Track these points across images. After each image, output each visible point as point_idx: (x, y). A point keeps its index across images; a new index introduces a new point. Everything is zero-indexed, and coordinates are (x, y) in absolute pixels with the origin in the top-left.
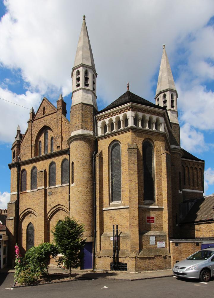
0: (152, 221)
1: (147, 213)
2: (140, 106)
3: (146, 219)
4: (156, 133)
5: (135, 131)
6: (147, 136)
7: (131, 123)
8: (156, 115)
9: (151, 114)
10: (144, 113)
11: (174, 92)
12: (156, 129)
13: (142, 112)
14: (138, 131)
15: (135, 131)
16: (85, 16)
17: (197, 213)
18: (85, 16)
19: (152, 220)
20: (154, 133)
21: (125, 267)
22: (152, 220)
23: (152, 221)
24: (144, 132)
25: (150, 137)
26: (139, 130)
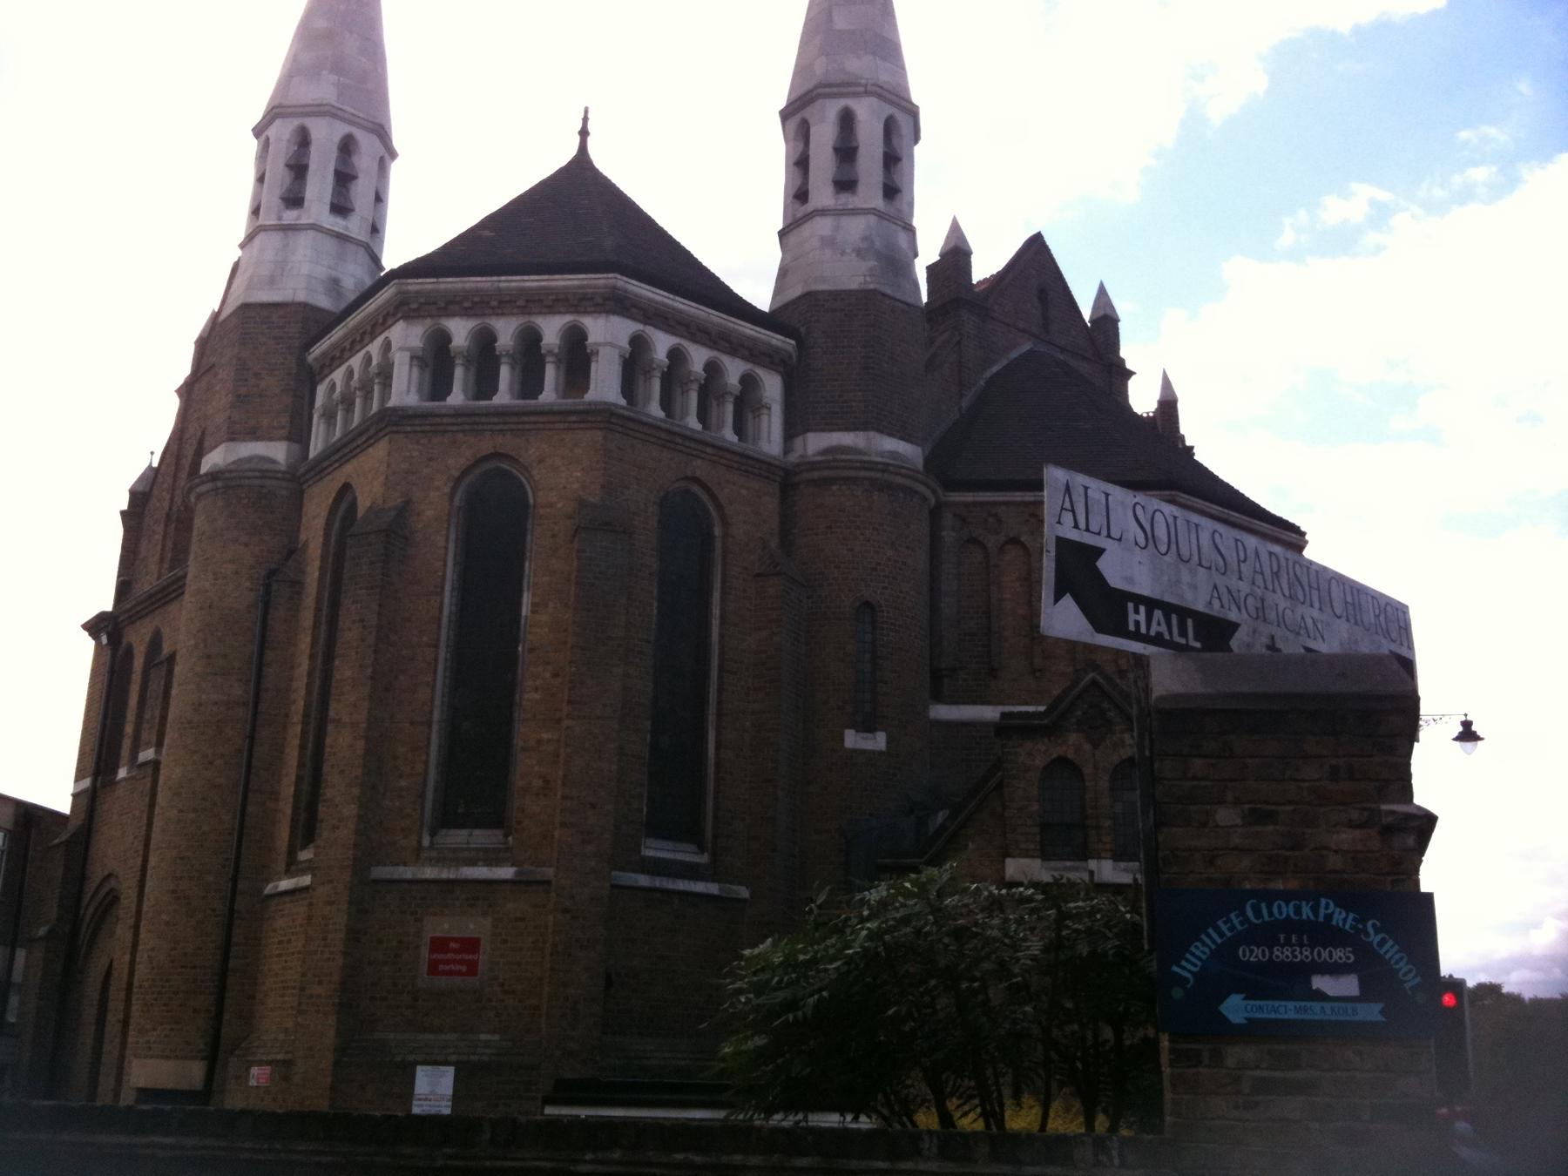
0: (464, 969)
1: (435, 914)
2: (449, 286)
3: (425, 952)
4: (544, 419)
5: (409, 429)
6: (486, 446)
7: (605, 385)
8: (560, 313)
9: (525, 310)
10: (484, 315)
11: (855, 95)
12: (624, 397)
13: (467, 313)
14: (428, 428)
15: (409, 429)
16: (586, 112)
17: (1142, 399)
18: (586, 112)
19: (461, 962)
20: (532, 419)
21: (1029, 497)
22: (461, 962)
23: (464, 969)
24: (467, 427)
25: (506, 443)
26: (438, 420)
